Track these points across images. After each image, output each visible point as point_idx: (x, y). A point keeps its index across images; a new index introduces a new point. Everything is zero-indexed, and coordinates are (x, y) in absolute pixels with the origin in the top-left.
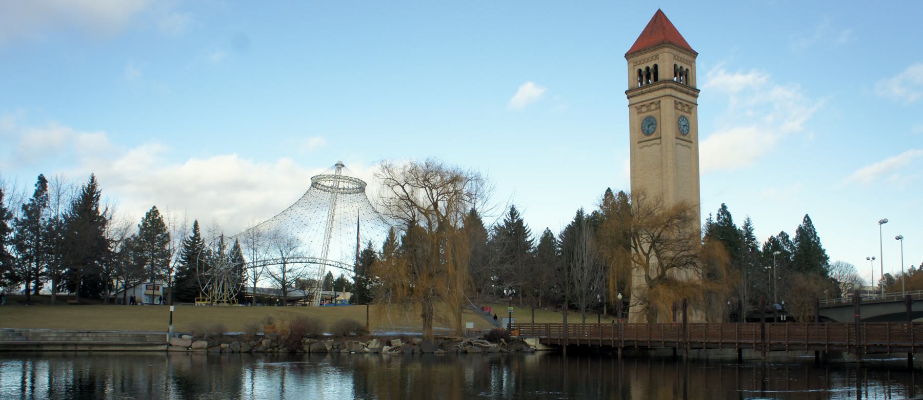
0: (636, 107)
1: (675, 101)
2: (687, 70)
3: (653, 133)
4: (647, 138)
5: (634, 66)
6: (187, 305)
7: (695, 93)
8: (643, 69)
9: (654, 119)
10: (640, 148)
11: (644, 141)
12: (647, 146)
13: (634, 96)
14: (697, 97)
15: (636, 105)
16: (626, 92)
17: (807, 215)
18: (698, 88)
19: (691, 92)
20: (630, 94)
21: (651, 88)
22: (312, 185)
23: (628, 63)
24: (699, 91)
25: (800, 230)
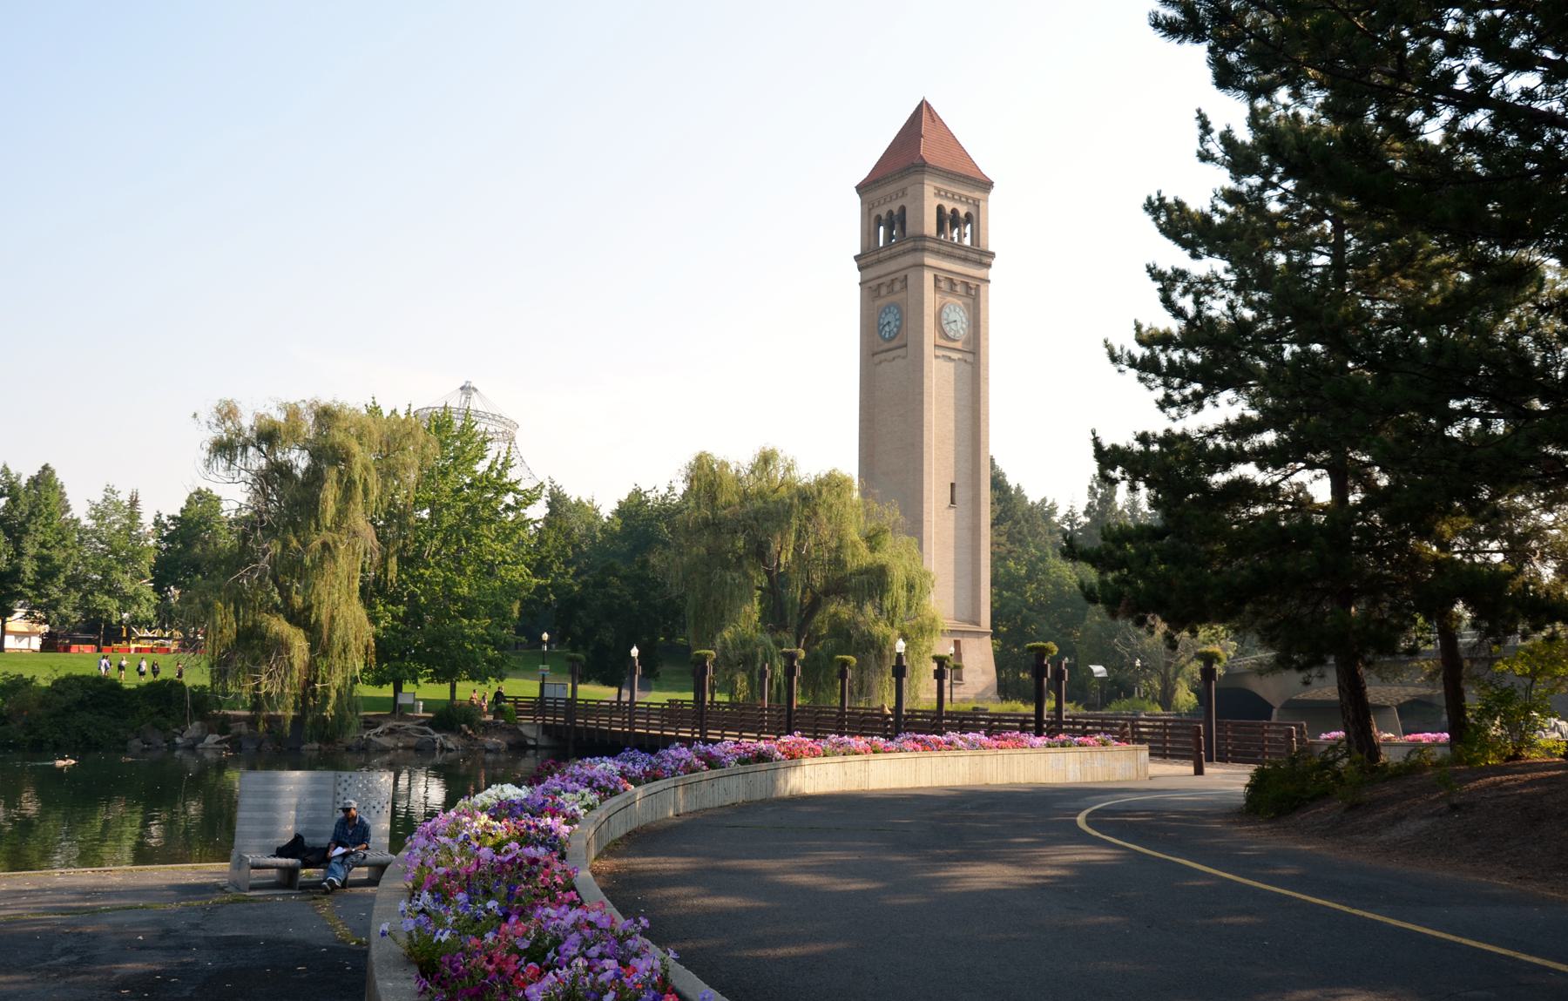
1: (935, 276)
4: (887, 346)
6: (912, 788)
11: (883, 352)
12: (886, 360)
14: (989, 266)
16: (857, 258)
18: (991, 249)
20: (863, 262)
21: (893, 250)
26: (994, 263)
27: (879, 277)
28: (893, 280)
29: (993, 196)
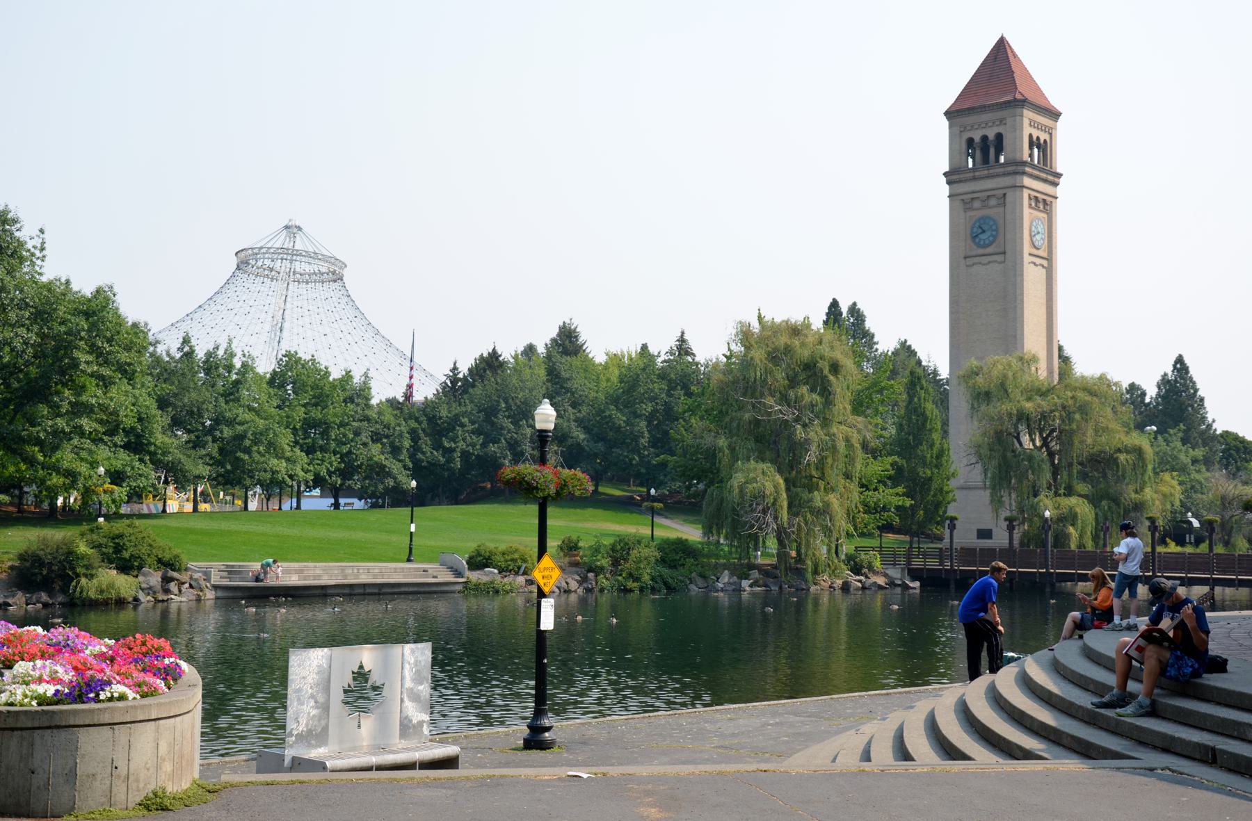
0: (963, 200)
2: (1045, 141)
3: (991, 244)
5: (961, 132)
7: (1056, 180)
8: (977, 138)
9: (994, 221)
10: (967, 266)
11: (976, 256)
12: (980, 263)
13: (960, 181)
14: (1056, 184)
15: (962, 197)
16: (945, 174)
17: (1180, 356)
18: (1059, 171)
19: (1050, 178)
20: (954, 177)
21: (991, 171)
22: (238, 268)
23: (951, 127)
24: (1061, 175)
25: (1164, 382)
26: (1062, 180)
27: (974, 192)
28: (972, 199)
29: (1061, 125)
